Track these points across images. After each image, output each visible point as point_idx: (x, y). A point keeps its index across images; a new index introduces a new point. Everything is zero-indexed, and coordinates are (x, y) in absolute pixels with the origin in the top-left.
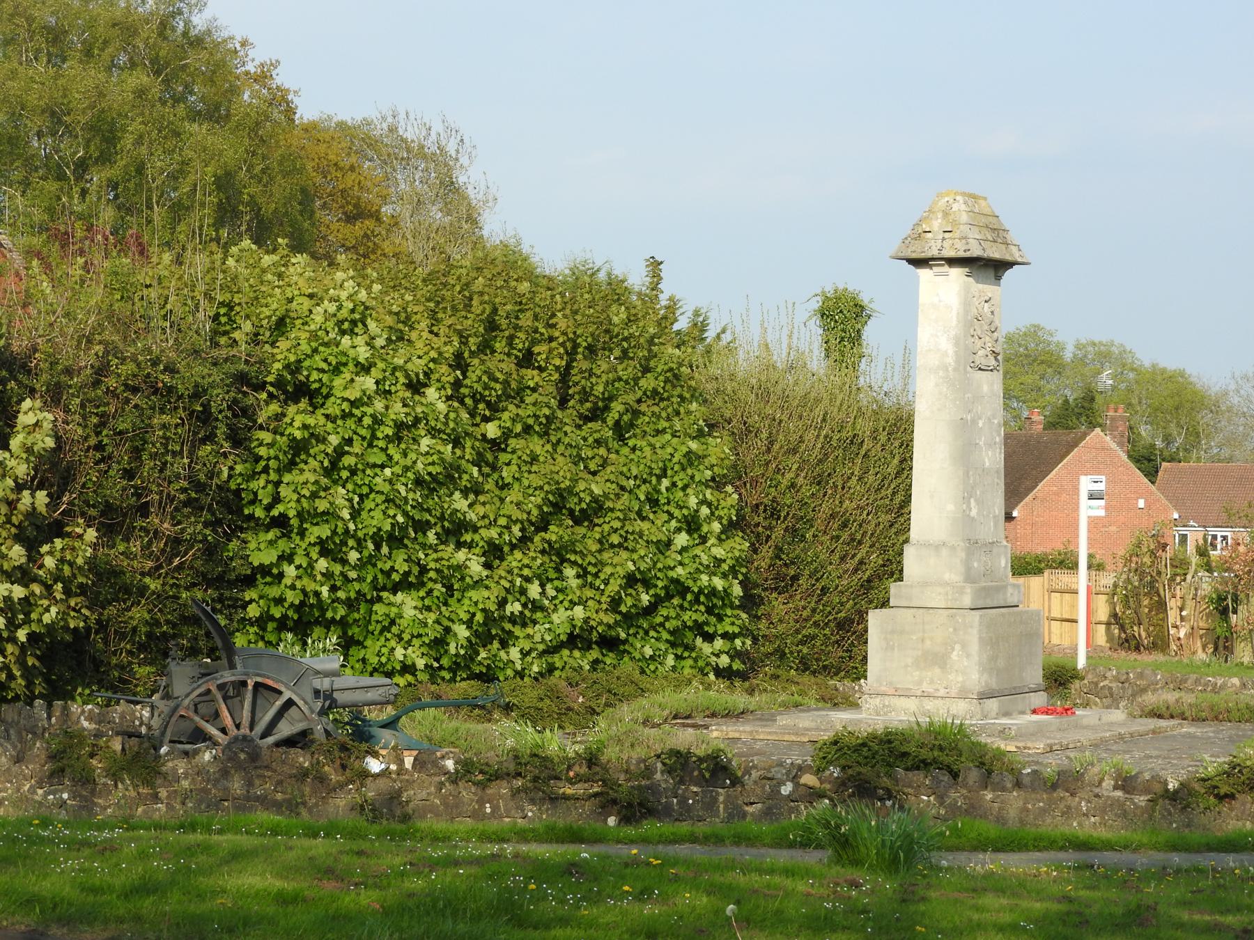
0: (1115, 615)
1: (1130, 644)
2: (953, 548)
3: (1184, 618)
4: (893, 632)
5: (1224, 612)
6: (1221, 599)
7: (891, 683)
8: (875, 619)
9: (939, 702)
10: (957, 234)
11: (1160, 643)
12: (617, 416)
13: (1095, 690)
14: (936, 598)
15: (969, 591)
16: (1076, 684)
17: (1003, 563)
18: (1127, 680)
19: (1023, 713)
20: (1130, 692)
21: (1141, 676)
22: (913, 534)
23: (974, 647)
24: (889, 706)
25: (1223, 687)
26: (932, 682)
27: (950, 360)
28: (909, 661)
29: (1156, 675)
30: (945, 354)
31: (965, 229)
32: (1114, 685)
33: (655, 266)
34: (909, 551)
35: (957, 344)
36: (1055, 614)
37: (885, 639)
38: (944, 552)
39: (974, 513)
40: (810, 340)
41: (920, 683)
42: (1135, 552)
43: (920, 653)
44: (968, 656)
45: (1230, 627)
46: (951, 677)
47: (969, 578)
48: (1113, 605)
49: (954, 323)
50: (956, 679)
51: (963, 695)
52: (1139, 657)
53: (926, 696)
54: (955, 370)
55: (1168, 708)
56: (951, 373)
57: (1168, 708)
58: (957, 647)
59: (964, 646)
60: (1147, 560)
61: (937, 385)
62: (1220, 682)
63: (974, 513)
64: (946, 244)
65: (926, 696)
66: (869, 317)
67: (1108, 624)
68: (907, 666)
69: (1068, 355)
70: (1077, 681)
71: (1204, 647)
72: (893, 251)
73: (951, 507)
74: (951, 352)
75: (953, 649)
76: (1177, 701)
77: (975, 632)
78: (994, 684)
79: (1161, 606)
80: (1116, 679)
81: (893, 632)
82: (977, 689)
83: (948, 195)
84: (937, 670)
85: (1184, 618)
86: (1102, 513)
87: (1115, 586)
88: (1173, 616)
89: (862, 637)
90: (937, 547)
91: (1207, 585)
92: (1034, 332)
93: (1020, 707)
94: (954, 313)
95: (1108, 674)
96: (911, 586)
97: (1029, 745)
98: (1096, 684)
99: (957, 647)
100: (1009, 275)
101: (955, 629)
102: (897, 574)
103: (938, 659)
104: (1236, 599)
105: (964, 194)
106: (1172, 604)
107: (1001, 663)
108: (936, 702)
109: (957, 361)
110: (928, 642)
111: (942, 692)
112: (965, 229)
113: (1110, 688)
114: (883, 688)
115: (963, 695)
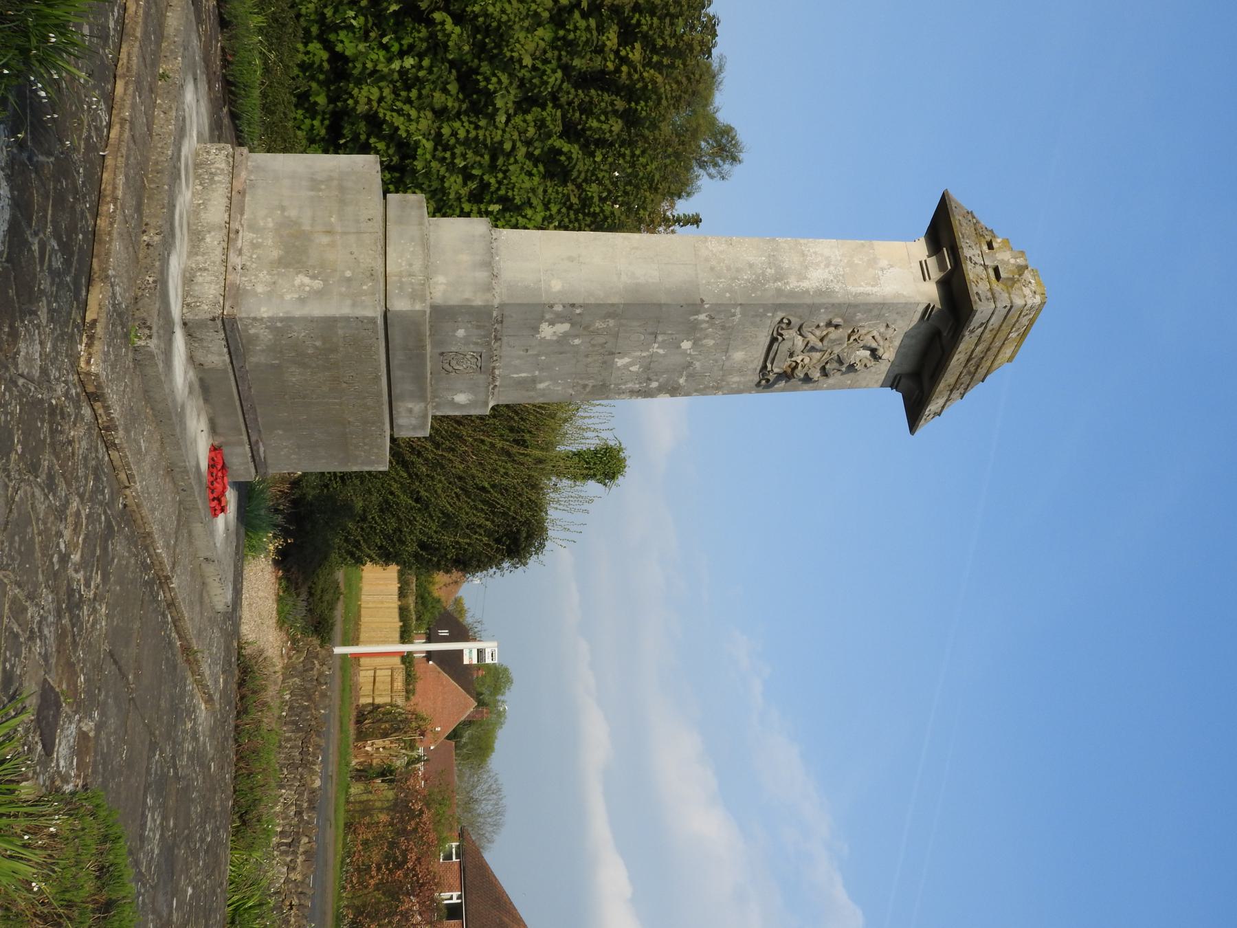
0: (379, 706)
1: (360, 718)
2: (489, 288)
3: (377, 749)
4: (342, 189)
5: (382, 774)
6: (391, 772)
7: (253, 186)
8: (366, 167)
9: (217, 255)
10: (998, 287)
11: (362, 736)
12: (565, 149)
13: (312, 656)
14: (403, 258)
15: (418, 307)
16: (316, 641)
17: (461, 398)
18: (320, 684)
19: (213, 429)
20: (309, 686)
21: (324, 695)
22: (507, 234)
23: (317, 310)
24: (212, 181)
25: (312, 772)
26: (255, 246)
27: (793, 284)
28: (293, 213)
29: (324, 709)
30: (802, 277)
31: (1004, 301)
32: (315, 672)
33: (695, 221)
34: (478, 226)
35: (819, 293)
36: (378, 672)
37: (330, 179)
38: (482, 275)
39: (547, 331)
40: (590, 442)
41: (252, 227)
42: (419, 717)
43: (307, 228)
44: (302, 301)
45: (373, 778)
46: (264, 275)
47: (443, 314)
48: (386, 704)
49: (853, 289)
50: (259, 282)
51: (231, 292)
52: (352, 722)
53: (230, 236)
54: (779, 292)
55: (254, 692)
56: (772, 286)
57: (254, 692)
58: (317, 284)
59: (319, 294)
60: (414, 724)
61: (751, 266)
62: (317, 768)
63: (547, 331)
64: (980, 269)
65: (230, 236)
66: (605, 485)
67: (373, 704)
68: (283, 209)
69: (499, 697)
70: (319, 642)
71: (361, 764)
72: (957, 196)
73: (556, 285)
74: (805, 285)
75: (314, 277)
76: (265, 704)
77: (346, 310)
78: (257, 358)
79: (385, 735)
80: (321, 674)
81: (342, 189)
82: (241, 313)
83: (1038, 283)
84: (275, 254)
85: (377, 749)
86: (466, 661)
87: (397, 707)
88: (379, 743)
89: (332, 143)
90: (488, 263)
91: (399, 763)
92: (509, 681)
93: (221, 421)
94: (868, 289)
95: (325, 668)
96: (421, 224)
97: (98, 346)
98: (316, 657)
99: (317, 284)
100: (896, 399)
101: (349, 280)
102: (441, 207)
103: (294, 252)
104: (391, 781)
105: (1043, 303)
106: (387, 742)
107: (294, 376)
108: (218, 251)
109: (792, 294)
110: (325, 240)
111: (234, 259)
112: (1004, 301)
113: (312, 669)
114: (244, 174)
115: (231, 292)
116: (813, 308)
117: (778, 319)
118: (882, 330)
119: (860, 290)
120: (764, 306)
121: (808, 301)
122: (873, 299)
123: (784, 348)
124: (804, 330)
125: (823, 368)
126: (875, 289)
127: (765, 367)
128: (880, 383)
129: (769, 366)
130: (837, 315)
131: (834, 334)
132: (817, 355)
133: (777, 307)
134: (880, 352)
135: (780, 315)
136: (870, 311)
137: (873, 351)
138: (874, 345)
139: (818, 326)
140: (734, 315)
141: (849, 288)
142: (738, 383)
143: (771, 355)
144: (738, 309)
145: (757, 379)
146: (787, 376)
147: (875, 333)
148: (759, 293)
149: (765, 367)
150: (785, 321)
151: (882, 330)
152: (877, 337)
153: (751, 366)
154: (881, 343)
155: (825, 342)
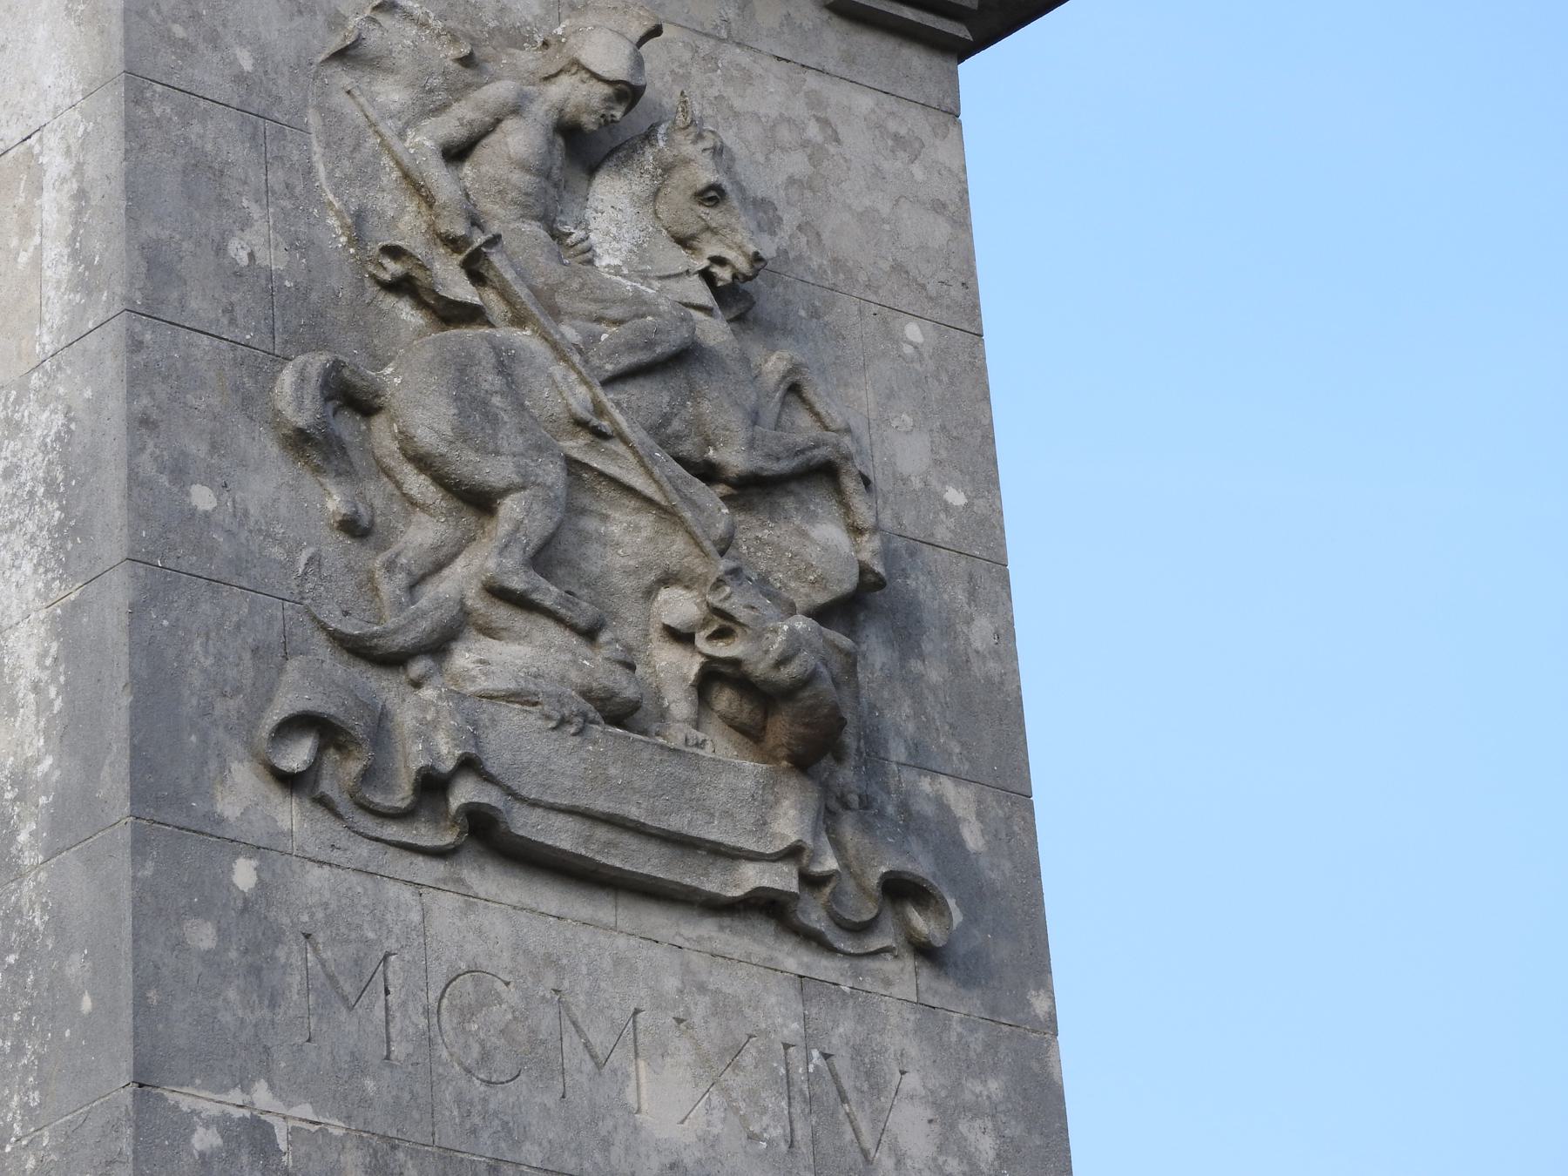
54: (69, 824)
94: (53, 209)
116: (169, 559)
117: (290, 814)
118: (392, 93)
119: (57, 265)
120: (153, 911)
121: (118, 592)
122: (107, 161)
123: (550, 772)
124: (400, 625)
125: (752, 490)
126: (55, 163)
127: (767, 908)
128: (915, 122)
129: (751, 878)
130: (252, 402)
131: (420, 405)
132: (623, 539)
133: (165, 810)
134: (571, 93)
135: (241, 794)
136: (203, 171)
137: (583, 148)
138: (519, 141)
139: (353, 528)
140: (256, 1134)
141: (47, 340)
142: (947, 1113)
143: (648, 862)
144: (204, 1105)
145: (902, 978)
146: (803, 727)
147: (424, 141)
148: (76, 966)
149: (767, 908)
150: (298, 755)
151: (392, 93)
152: (450, 126)
153: (781, 1015)
154: (498, 91)
155: (493, 471)
